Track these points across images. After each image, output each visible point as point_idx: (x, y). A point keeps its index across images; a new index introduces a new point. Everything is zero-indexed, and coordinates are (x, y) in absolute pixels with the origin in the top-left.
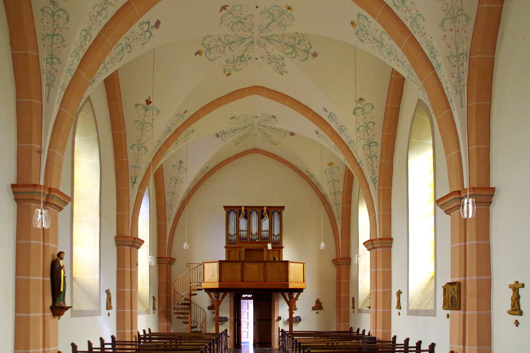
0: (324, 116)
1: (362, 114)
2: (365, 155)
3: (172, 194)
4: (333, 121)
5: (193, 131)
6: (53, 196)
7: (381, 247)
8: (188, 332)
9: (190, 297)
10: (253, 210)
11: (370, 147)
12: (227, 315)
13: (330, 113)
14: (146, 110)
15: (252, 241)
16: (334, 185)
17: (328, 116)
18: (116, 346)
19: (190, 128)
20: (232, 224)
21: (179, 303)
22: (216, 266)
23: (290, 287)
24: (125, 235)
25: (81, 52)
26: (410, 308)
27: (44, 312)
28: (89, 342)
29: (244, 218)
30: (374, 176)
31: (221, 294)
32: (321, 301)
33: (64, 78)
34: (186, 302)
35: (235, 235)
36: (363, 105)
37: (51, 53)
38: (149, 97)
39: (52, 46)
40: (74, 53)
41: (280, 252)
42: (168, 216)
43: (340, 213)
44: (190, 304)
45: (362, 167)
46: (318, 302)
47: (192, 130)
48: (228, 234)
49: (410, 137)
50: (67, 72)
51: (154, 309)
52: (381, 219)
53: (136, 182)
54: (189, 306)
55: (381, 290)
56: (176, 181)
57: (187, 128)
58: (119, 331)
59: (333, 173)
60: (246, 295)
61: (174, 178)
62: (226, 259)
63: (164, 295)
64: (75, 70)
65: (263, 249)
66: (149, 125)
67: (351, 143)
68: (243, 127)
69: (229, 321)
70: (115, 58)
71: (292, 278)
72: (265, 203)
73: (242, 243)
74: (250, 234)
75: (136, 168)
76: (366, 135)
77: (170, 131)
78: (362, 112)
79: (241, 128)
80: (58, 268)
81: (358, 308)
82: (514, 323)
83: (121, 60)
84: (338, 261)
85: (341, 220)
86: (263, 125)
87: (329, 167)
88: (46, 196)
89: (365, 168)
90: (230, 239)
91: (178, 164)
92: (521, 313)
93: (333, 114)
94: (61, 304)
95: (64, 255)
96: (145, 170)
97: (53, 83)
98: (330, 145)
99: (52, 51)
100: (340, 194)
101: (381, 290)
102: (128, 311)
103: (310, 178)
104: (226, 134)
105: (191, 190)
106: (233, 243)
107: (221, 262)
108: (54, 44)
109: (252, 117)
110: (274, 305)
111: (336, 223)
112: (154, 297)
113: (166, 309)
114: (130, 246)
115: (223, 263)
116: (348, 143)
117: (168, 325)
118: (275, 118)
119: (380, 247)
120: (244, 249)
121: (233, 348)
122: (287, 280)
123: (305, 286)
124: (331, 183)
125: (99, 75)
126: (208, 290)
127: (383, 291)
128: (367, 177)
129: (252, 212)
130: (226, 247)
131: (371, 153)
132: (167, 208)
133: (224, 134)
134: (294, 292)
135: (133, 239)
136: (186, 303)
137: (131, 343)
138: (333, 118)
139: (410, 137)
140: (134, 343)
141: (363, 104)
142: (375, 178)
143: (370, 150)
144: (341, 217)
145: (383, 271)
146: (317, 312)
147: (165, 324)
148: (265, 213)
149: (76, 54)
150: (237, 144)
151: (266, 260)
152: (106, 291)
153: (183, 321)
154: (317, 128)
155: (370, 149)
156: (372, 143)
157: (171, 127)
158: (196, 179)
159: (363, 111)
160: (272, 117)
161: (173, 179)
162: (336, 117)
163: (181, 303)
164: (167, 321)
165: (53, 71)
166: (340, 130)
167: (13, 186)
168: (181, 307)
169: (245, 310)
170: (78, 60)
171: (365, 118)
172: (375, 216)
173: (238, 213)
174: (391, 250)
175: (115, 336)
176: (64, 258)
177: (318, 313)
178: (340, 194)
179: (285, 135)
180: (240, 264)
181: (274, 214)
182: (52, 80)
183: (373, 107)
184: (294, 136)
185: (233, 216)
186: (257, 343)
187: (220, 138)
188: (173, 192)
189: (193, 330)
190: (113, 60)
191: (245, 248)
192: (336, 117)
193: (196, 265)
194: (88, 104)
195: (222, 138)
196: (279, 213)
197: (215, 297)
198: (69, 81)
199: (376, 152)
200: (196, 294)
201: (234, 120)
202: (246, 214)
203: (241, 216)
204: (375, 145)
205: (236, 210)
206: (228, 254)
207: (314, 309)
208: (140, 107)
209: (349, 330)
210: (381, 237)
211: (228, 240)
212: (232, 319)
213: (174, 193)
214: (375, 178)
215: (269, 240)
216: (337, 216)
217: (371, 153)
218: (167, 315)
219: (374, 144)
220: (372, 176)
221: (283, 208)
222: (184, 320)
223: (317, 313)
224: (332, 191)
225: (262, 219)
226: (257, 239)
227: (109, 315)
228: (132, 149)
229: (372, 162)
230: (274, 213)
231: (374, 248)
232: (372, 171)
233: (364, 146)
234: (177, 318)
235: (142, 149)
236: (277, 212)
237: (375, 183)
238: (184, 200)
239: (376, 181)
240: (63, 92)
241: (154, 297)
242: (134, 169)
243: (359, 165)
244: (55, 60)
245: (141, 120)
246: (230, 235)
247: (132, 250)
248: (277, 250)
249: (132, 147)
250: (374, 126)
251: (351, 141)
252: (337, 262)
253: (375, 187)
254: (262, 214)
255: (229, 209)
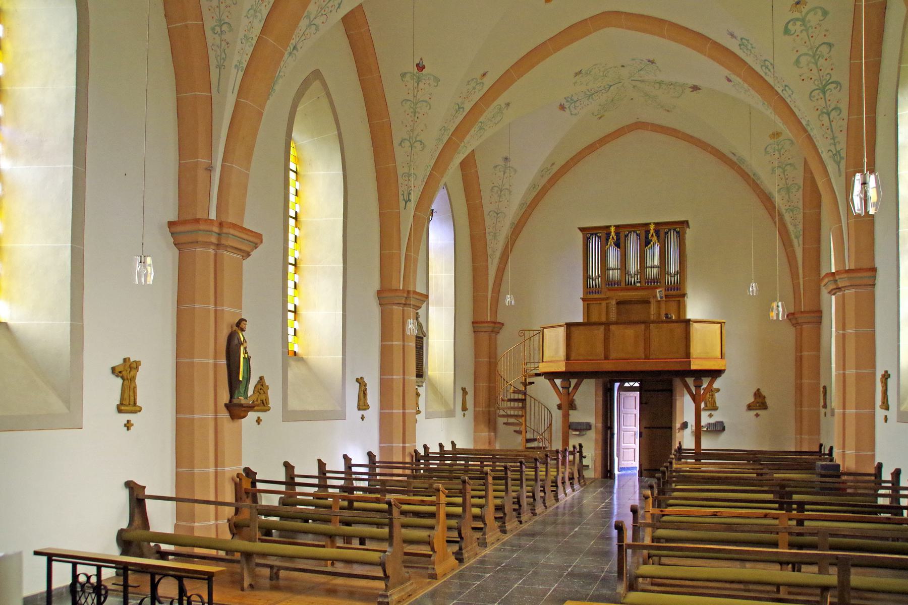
0: (733, 46)
1: (804, 32)
2: (816, 109)
3: (496, 215)
4: (749, 53)
5: (508, 105)
6: (226, 234)
7: (851, 286)
8: (521, 448)
9: (526, 389)
10: (630, 232)
11: (824, 93)
12: (591, 420)
13: (742, 39)
14: (419, 81)
15: (630, 286)
16: (784, 174)
17: (740, 45)
18: (377, 469)
19: (501, 100)
20: (594, 260)
21: (506, 398)
22: (562, 331)
23: (693, 367)
24: (393, 288)
25: (263, 7)
26: (902, 408)
27: (216, 412)
28: (319, 461)
29: (615, 246)
30: (836, 149)
31: (573, 382)
32: (764, 392)
33: (239, 52)
34: (516, 396)
35: (599, 277)
36: (803, 14)
37: (219, 17)
38: (421, 59)
39: (219, 6)
40: (252, 12)
41: (681, 305)
42: (489, 252)
43: (800, 227)
44: (525, 400)
45: (812, 134)
46: (758, 394)
47: (506, 104)
48: (586, 277)
49: (900, 62)
50: (243, 41)
51: (464, 409)
52: (852, 232)
53: (409, 200)
54: (523, 403)
55: (854, 371)
56: (501, 192)
57: (494, 100)
58: (382, 445)
59: (782, 151)
60: (632, 384)
61: (497, 187)
62: (583, 319)
63: (483, 384)
64: (256, 36)
65: (648, 299)
66: (425, 104)
67: (786, 90)
68: (604, 87)
69: (594, 430)
70: (327, 6)
71: (698, 351)
72: (652, 218)
73: (610, 290)
74: (625, 274)
75: (409, 177)
76: (815, 71)
77: (461, 110)
78: (803, 28)
79: (601, 89)
80: (236, 345)
81: (831, 407)
82: (132, 425)
83: (338, 7)
84: (796, 316)
85: (801, 238)
86: (640, 79)
87: (772, 141)
88: (218, 235)
89: (815, 133)
90: (668, 282)
91: (502, 163)
92: (137, 410)
93: (746, 40)
94: (241, 399)
95: (245, 324)
96: (424, 178)
97: (223, 62)
98: (754, 99)
99: (220, 14)
100: (798, 189)
101: (854, 371)
102: (398, 411)
103: (740, 165)
104: (577, 102)
105: (528, 204)
106: (595, 292)
107: (569, 326)
108: (222, 3)
109: (615, 67)
110: (676, 400)
111: (792, 246)
112: (464, 390)
113: (487, 409)
114: (402, 305)
115: (573, 329)
116: (783, 90)
117: (489, 435)
118: (654, 64)
119: (848, 286)
120: (614, 302)
121: (600, 477)
122: (688, 355)
123: (725, 366)
124: (778, 171)
125: (303, 38)
126: (551, 376)
127: (857, 374)
128: (822, 152)
129: (628, 234)
130: (583, 300)
131: (826, 105)
132: (489, 238)
133: (573, 104)
134: (705, 377)
135: (406, 293)
136: (516, 397)
137: (402, 465)
138: (748, 47)
139: (900, 62)
140: (407, 465)
141: (804, 11)
142: (839, 152)
143: (825, 99)
144: (801, 233)
145: (856, 333)
146: (757, 413)
147: (485, 434)
148: (652, 235)
149: (255, 11)
150: (600, 118)
151: (655, 318)
152: (357, 379)
153: (515, 429)
154: (727, 72)
155: (825, 96)
156: (829, 84)
157: (463, 103)
158: (534, 186)
159: (804, 24)
160: (648, 63)
161: (495, 188)
162: (751, 44)
163: (509, 397)
164: (489, 428)
165: (224, 43)
166: (764, 68)
167: (171, 224)
168: (509, 405)
169: (629, 410)
170: (260, 21)
171: (810, 37)
172: (841, 228)
173: (604, 238)
174: (874, 291)
175: (376, 452)
176: (247, 329)
177: (712, 415)
178: (798, 189)
179: (683, 92)
180: (602, 328)
181: (668, 236)
182: (223, 58)
183: (825, 13)
184: (699, 91)
185: (595, 244)
186: (645, 470)
187: (567, 110)
188: (496, 211)
189: (530, 445)
190: (325, 11)
191: (616, 299)
192: (751, 44)
193: (532, 333)
194: (317, 84)
195: (571, 111)
196: (678, 233)
197: (562, 388)
198: (249, 56)
199: (838, 102)
200: (533, 383)
201: (582, 76)
202: (618, 239)
203: (609, 244)
204: (835, 88)
205: (639, 230)
206: (587, 311)
207: (750, 407)
208: (408, 77)
209: (817, 450)
210: (852, 267)
211: (587, 287)
212: (600, 425)
213: (499, 211)
214: (839, 152)
215: (660, 282)
216: (793, 231)
217: (826, 105)
218: (489, 419)
219: (832, 86)
220: (832, 148)
221: (685, 223)
222: (518, 428)
223: (757, 415)
224: (781, 186)
225: (647, 245)
226: (637, 282)
227: (363, 418)
228: (402, 147)
229: (831, 122)
230: (668, 233)
231: (839, 289)
232: (831, 139)
233: (811, 93)
234: (504, 423)
235: (418, 144)
236: (675, 232)
237: (840, 162)
238: (516, 222)
239: (841, 158)
240: (241, 74)
241: (465, 388)
242: (407, 178)
243: (805, 131)
244: (225, 27)
245: (410, 97)
246: (591, 277)
247: (406, 313)
248: (674, 301)
249: (401, 143)
250: (830, 51)
251: (786, 86)
252: (796, 319)
253: (839, 170)
254: (647, 237)
255: (588, 233)
